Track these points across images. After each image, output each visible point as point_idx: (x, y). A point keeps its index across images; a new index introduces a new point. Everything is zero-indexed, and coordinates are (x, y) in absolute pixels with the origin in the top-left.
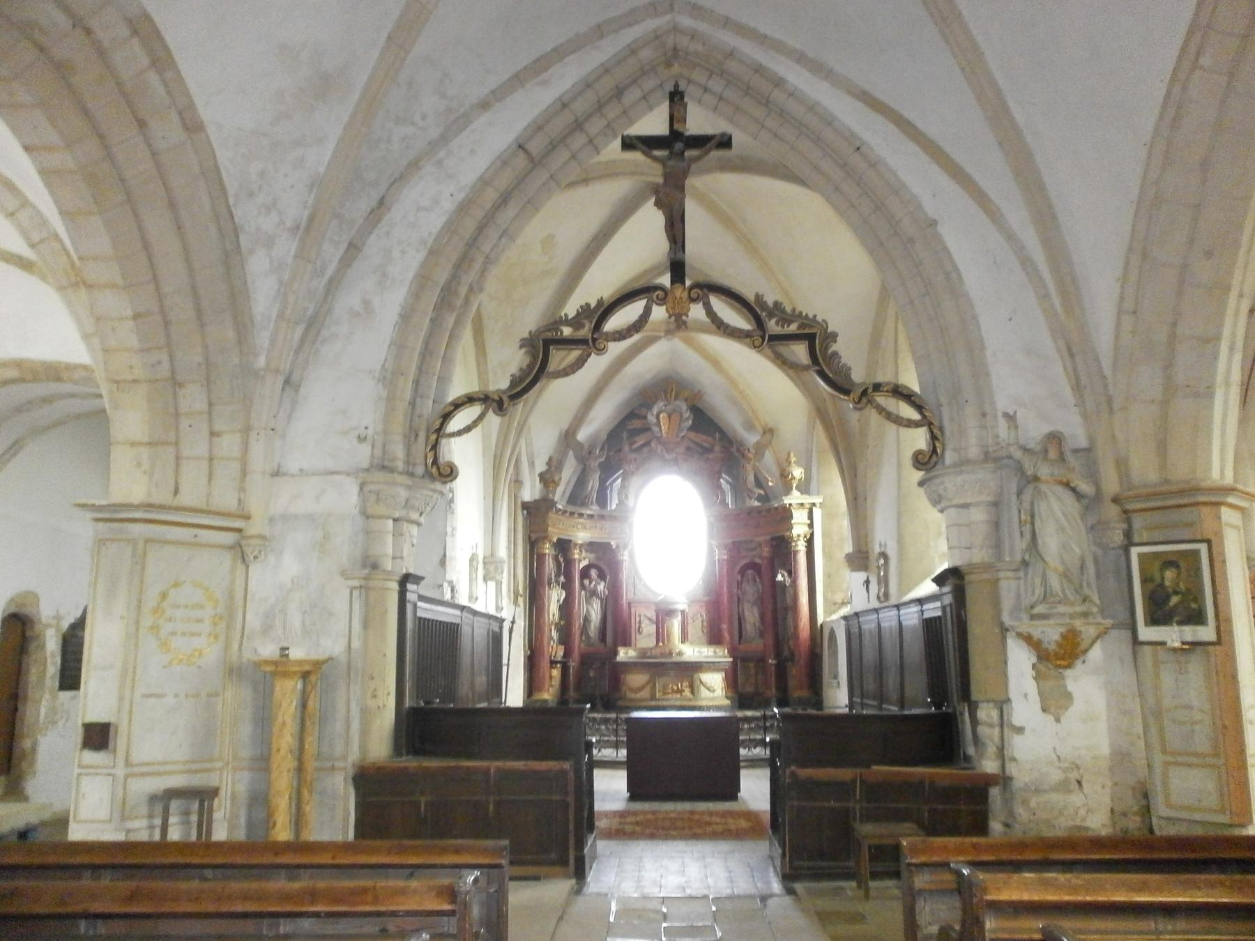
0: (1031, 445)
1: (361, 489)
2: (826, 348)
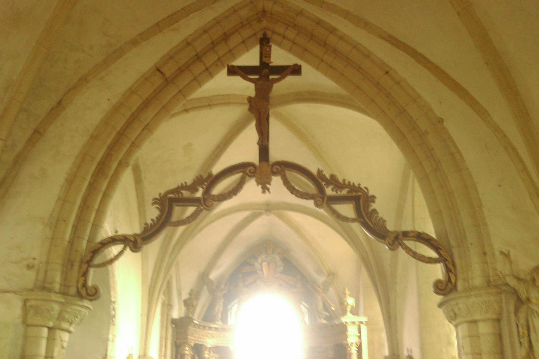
0: (522, 276)
1: (25, 305)
2: (368, 206)
